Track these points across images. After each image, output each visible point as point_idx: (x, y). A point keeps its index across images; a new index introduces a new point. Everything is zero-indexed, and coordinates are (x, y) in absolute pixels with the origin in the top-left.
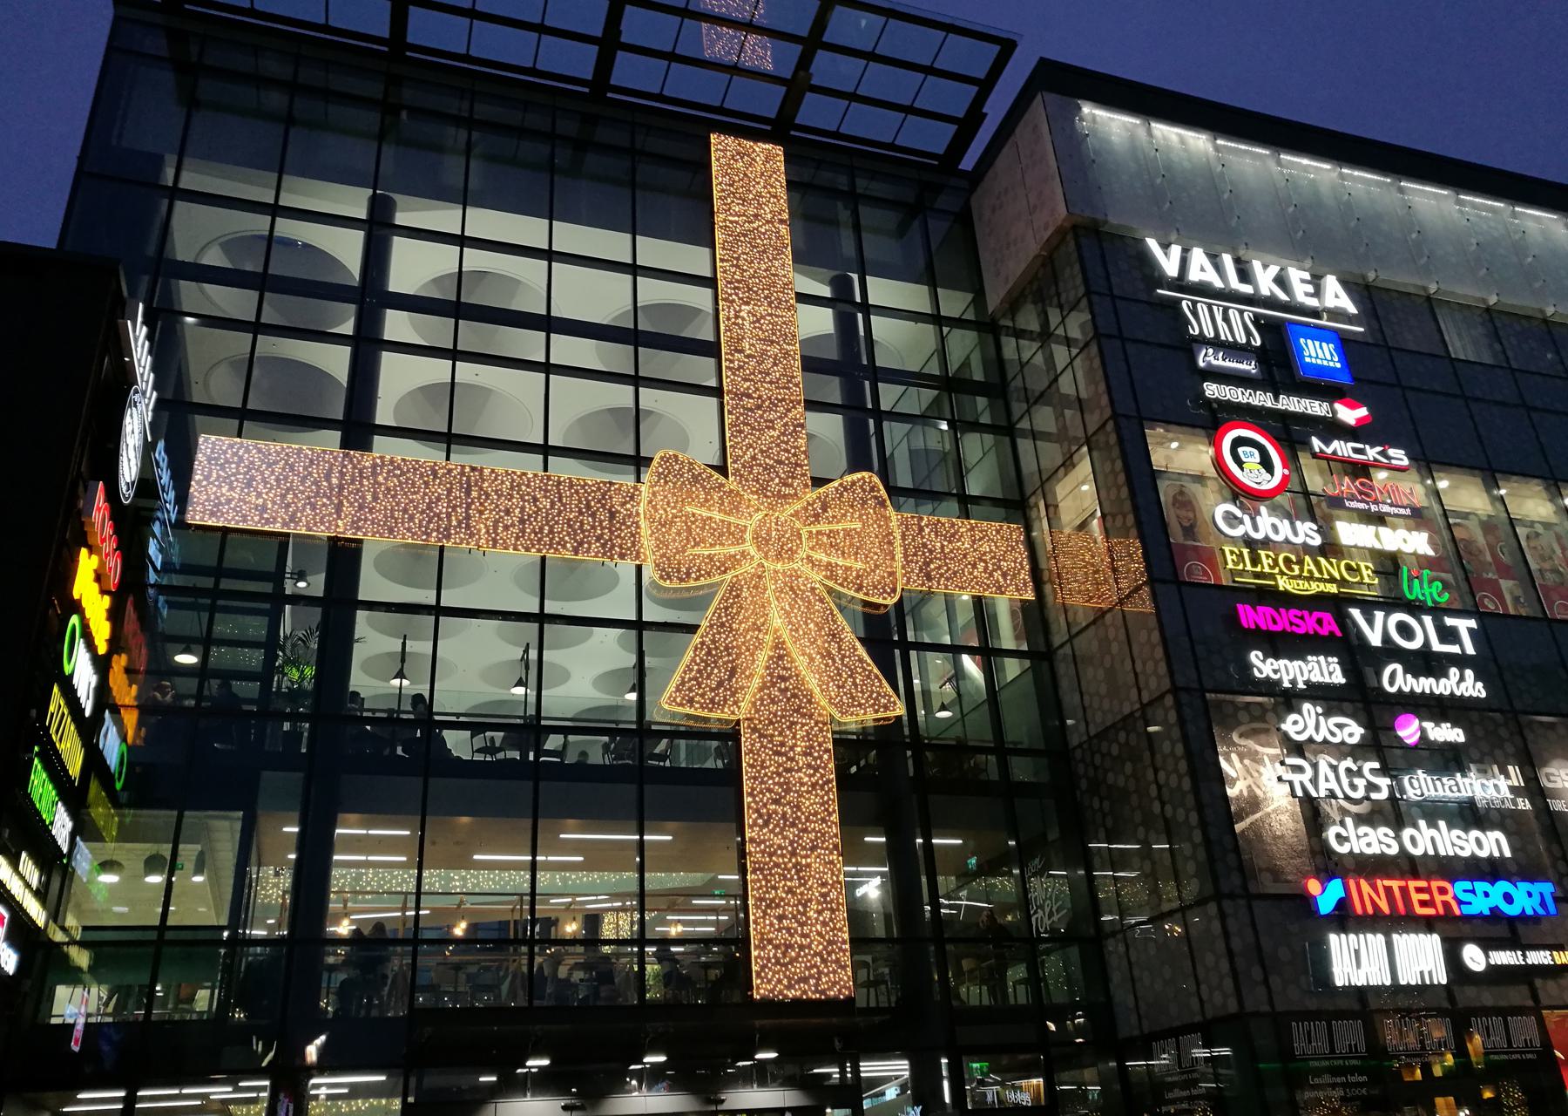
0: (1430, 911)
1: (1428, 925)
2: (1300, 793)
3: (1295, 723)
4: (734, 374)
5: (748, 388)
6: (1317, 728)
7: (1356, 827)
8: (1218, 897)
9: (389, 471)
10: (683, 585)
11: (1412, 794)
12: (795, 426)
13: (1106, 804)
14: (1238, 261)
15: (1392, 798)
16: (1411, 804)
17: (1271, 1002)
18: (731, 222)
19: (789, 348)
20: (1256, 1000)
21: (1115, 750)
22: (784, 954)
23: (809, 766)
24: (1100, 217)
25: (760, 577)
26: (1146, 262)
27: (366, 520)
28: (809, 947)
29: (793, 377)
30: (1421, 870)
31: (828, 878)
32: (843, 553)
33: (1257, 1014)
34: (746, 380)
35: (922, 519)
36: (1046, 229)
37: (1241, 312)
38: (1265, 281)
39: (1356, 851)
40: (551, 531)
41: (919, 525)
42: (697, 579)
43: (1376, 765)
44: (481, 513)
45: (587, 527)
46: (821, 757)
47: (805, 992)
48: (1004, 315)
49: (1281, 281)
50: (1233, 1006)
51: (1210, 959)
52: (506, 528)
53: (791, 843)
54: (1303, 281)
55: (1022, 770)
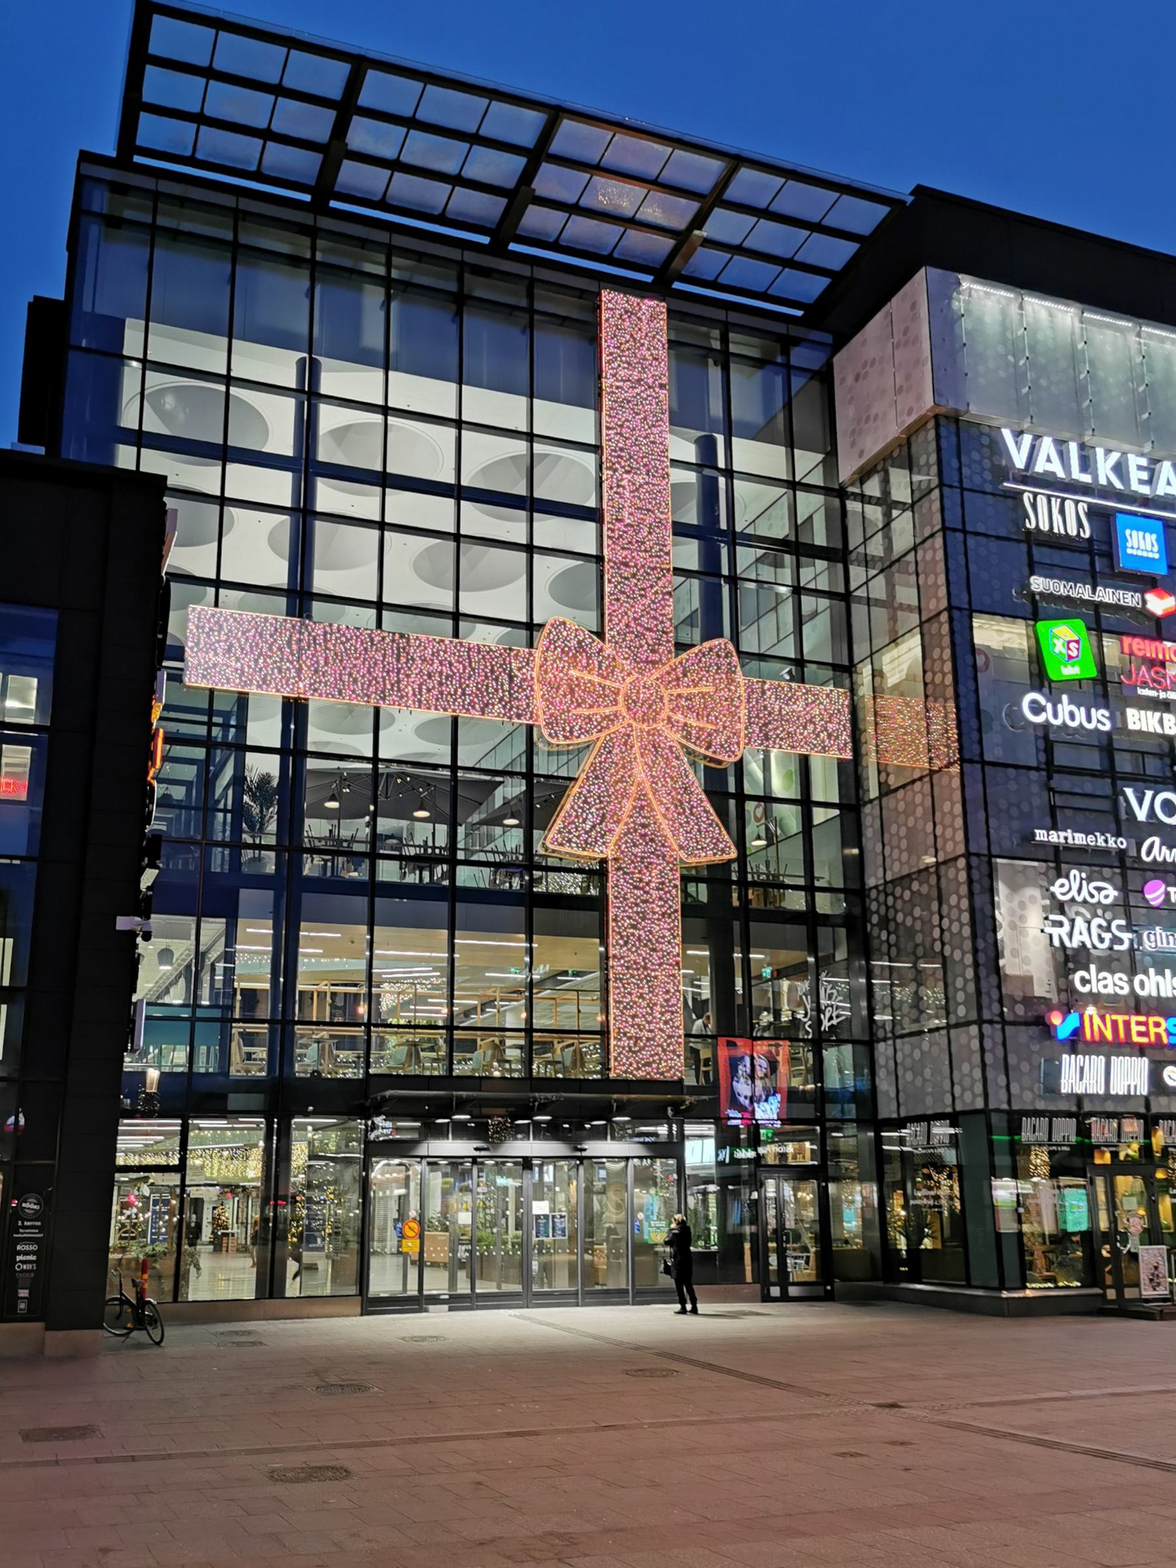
0: (1144, 1040)
1: (1141, 1050)
2: (1056, 943)
3: (1062, 886)
4: (614, 543)
5: (626, 557)
6: (1079, 891)
7: (1099, 971)
8: (980, 1022)
9: (337, 638)
10: (568, 742)
11: (1148, 945)
12: (664, 594)
13: (893, 938)
14: (1082, 447)
15: (1132, 950)
16: (1145, 954)
17: (1009, 1102)
18: (617, 388)
19: (662, 516)
20: (998, 1101)
21: (907, 895)
22: (635, 1044)
23: (661, 899)
24: (962, 408)
25: (629, 736)
26: (996, 447)
27: (320, 682)
28: (653, 1039)
29: (665, 546)
30: (1143, 1008)
31: (670, 987)
32: (698, 714)
33: (998, 1111)
34: (623, 548)
35: (765, 683)
36: (910, 413)
37: (1077, 502)
38: (1105, 472)
39: (1095, 990)
40: (464, 694)
41: (762, 688)
42: (578, 737)
43: (1123, 922)
44: (408, 676)
45: (490, 690)
46: (669, 892)
47: (648, 1073)
48: (852, 484)
49: (1120, 469)
50: (979, 1104)
51: (966, 1068)
52: (429, 690)
53: (644, 959)
54: (1140, 468)
55: (824, 904)
